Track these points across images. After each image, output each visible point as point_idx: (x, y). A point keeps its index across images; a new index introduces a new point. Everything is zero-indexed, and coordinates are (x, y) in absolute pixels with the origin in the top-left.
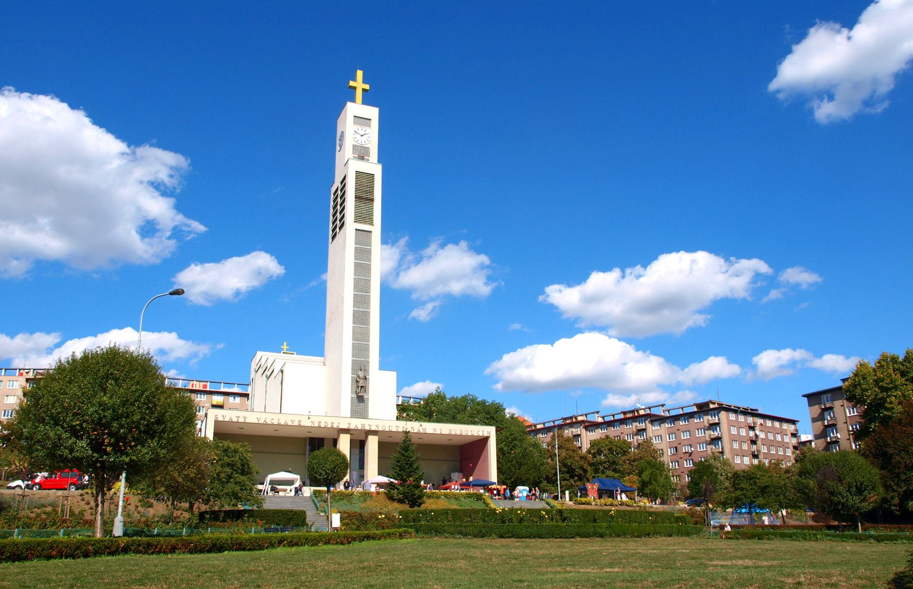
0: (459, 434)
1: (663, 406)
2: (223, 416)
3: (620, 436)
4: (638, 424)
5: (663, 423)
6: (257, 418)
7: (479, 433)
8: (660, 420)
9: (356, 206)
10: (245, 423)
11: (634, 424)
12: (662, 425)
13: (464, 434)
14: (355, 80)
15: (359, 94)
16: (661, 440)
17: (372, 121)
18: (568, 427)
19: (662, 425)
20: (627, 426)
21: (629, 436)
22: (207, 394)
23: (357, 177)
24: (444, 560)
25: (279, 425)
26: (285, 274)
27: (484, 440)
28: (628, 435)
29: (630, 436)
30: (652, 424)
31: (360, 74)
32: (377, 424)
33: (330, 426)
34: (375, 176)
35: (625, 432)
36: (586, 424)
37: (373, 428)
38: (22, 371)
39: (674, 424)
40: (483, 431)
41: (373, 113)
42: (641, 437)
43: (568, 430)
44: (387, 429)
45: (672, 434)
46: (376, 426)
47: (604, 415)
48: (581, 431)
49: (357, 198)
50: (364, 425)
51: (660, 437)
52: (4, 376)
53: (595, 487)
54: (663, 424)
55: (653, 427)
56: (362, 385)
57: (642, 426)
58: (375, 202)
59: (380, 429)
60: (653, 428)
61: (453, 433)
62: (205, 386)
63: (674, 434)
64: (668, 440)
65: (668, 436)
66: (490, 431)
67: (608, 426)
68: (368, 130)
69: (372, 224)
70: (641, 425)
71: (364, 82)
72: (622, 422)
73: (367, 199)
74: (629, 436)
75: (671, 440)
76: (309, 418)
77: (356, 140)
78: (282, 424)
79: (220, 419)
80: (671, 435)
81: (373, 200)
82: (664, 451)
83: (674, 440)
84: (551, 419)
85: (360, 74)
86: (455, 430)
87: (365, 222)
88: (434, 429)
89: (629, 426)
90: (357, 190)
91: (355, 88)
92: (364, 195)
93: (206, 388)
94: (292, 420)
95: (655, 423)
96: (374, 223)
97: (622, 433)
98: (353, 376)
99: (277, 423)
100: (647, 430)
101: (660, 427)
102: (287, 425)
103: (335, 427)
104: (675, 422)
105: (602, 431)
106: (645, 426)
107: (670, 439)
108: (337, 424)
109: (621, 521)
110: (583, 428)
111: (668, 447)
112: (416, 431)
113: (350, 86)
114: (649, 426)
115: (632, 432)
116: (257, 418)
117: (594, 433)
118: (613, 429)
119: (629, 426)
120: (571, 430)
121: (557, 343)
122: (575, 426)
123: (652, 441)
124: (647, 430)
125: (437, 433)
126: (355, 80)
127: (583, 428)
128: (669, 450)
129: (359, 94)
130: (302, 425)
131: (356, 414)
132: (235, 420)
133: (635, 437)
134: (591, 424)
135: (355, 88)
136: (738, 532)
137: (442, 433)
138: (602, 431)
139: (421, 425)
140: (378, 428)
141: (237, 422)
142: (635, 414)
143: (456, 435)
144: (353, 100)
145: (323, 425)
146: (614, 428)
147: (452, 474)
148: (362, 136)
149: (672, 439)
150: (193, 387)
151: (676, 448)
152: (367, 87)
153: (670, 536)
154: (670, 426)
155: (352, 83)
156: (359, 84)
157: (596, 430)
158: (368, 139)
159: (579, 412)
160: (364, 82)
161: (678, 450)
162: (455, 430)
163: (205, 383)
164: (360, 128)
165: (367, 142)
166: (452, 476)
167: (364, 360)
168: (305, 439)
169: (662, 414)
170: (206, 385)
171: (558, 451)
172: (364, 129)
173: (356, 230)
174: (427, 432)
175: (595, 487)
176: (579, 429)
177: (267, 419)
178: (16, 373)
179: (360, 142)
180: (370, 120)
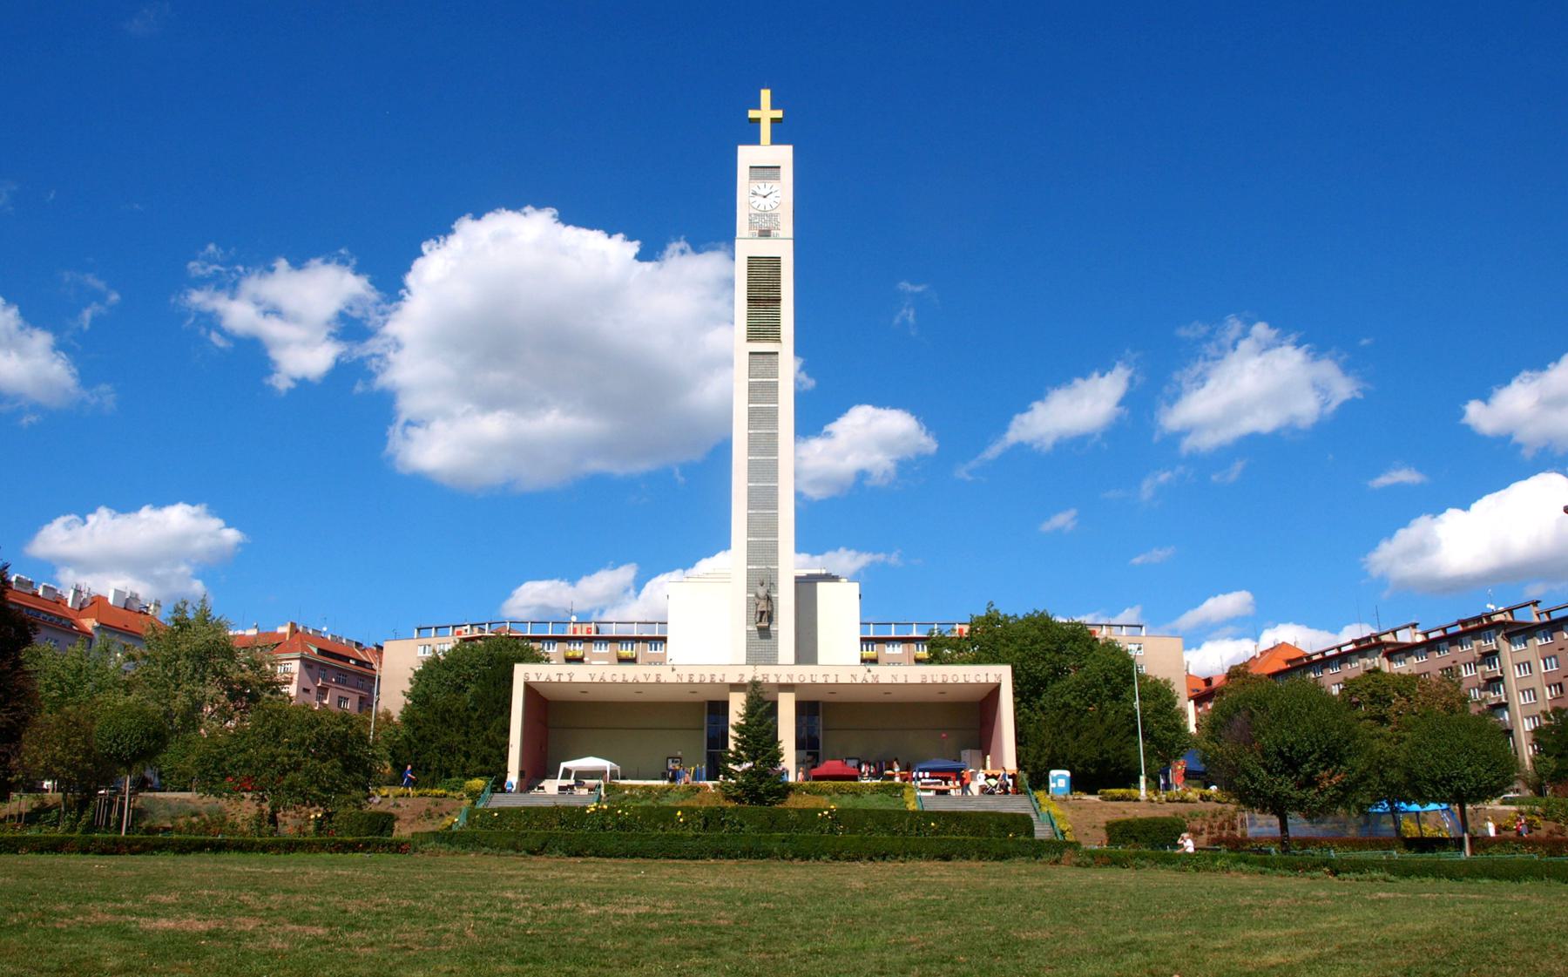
0: (940, 681)
1: (1535, 603)
2: (537, 674)
3: (1451, 668)
4: (1483, 642)
5: (1532, 637)
6: (590, 674)
7: (615, 678)
8: (1518, 632)
9: (750, 316)
10: (570, 683)
11: (1475, 643)
12: (1529, 642)
13: (950, 681)
14: (758, 107)
15: (765, 131)
16: (1530, 672)
17: (781, 169)
18: (1357, 656)
19: (1529, 641)
20: (1462, 648)
21: (1468, 666)
22: (585, 642)
23: (750, 267)
24: (123, 912)
25: (944, 684)
26: (938, 449)
27: (995, 690)
28: (1465, 666)
29: (1524, 668)
30: (1509, 641)
31: (765, 95)
32: (895, 674)
33: (708, 680)
34: (782, 259)
35: (1460, 660)
36: (1389, 649)
37: (783, 680)
38: (457, 629)
39: (1552, 639)
40: (987, 675)
41: (783, 155)
42: (1490, 668)
43: (1358, 662)
44: (808, 681)
45: (1550, 658)
46: (788, 675)
47: (1427, 629)
48: (1379, 661)
49: (751, 300)
50: (768, 675)
51: (1527, 665)
52: (435, 637)
53: (1179, 767)
54: (1531, 640)
55: (1513, 647)
56: (762, 610)
57: (1491, 645)
58: (782, 303)
59: (796, 681)
60: (1513, 649)
61: (929, 681)
62: (589, 631)
63: (1555, 657)
64: (1544, 670)
65: (1542, 662)
66: (1001, 675)
67: (1428, 651)
68: (775, 185)
69: (778, 340)
70: (1489, 643)
71: (774, 107)
72: (1453, 640)
73: (769, 300)
74: (1468, 666)
75: (1549, 670)
76: (673, 670)
77: (755, 205)
78: (630, 681)
79: (533, 679)
80: (1547, 660)
81: (778, 300)
82: (1538, 692)
83: (1555, 669)
84: (1335, 645)
85: (765, 95)
86: (932, 676)
87: (766, 339)
88: (788, 675)
89: (1467, 647)
90: (750, 288)
91: (758, 121)
92: (763, 295)
93: (590, 633)
94: (645, 675)
95: (1515, 638)
96: (782, 339)
97: (1454, 662)
98: (750, 595)
99: (621, 681)
100: (1500, 653)
101: (1526, 645)
102: (638, 683)
103: (718, 681)
104: (1555, 635)
105: (1418, 660)
106: (1497, 645)
107: (1546, 668)
108: (721, 677)
109: (843, 831)
110: (1383, 657)
111: (1544, 684)
112: (859, 681)
113: (750, 119)
114: (1504, 645)
115: (1473, 660)
116: (590, 674)
117: (1403, 665)
118: (1437, 656)
119: (1467, 647)
120: (1362, 661)
121: (1474, 506)
122: (1370, 653)
123: (1460, 673)
124: (1502, 653)
125: (899, 681)
126: (758, 107)
127: (1383, 657)
128: (1547, 689)
129: (765, 131)
130: (663, 681)
131: (753, 659)
132: (555, 679)
133: (1478, 667)
134: (1397, 648)
135: (758, 121)
136: (582, 862)
137: (909, 681)
138: (1418, 660)
139: (869, 671)
140: (792, 680)
141: (559, 682)
142: (1482, 622)
143: (955, 684)
144: (754, 140)
145: (696, 680)
146: (1439, 654)
147: (963, 752)
148: (765, 197)
149: (1552, 667)
150: (588, 633)
151: (1560, 684)
152: (779, 114)
153: (946, 858)
154: (1544, 642)
155: (752, 114)
156: (765, 113)
157: (1408, 659)
158: (777, 200)
159: (1382, 626)
160: (774, 107)
161: (1564, 690)
162: (932, 676)
163: (589, 626)
164: (762, 185)
165: (774, 205)
166: (962, 755)
167: (764, 567)
168: (703, 703)
169: (1536, 620)
170: (590, 629)
171: (1140, 705)
172: (768, 185)
173: (751, 353)
174: (881, 682)
175: (1179, 767)
176: (1376, 659)
177: (605, 675)
178: (548, 628)
179: (762, 208)
180: (779, 167)
